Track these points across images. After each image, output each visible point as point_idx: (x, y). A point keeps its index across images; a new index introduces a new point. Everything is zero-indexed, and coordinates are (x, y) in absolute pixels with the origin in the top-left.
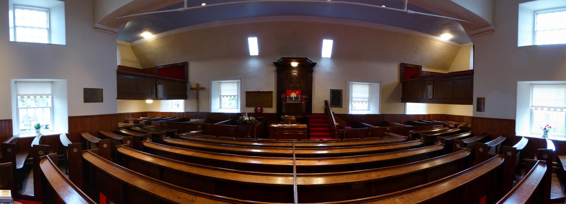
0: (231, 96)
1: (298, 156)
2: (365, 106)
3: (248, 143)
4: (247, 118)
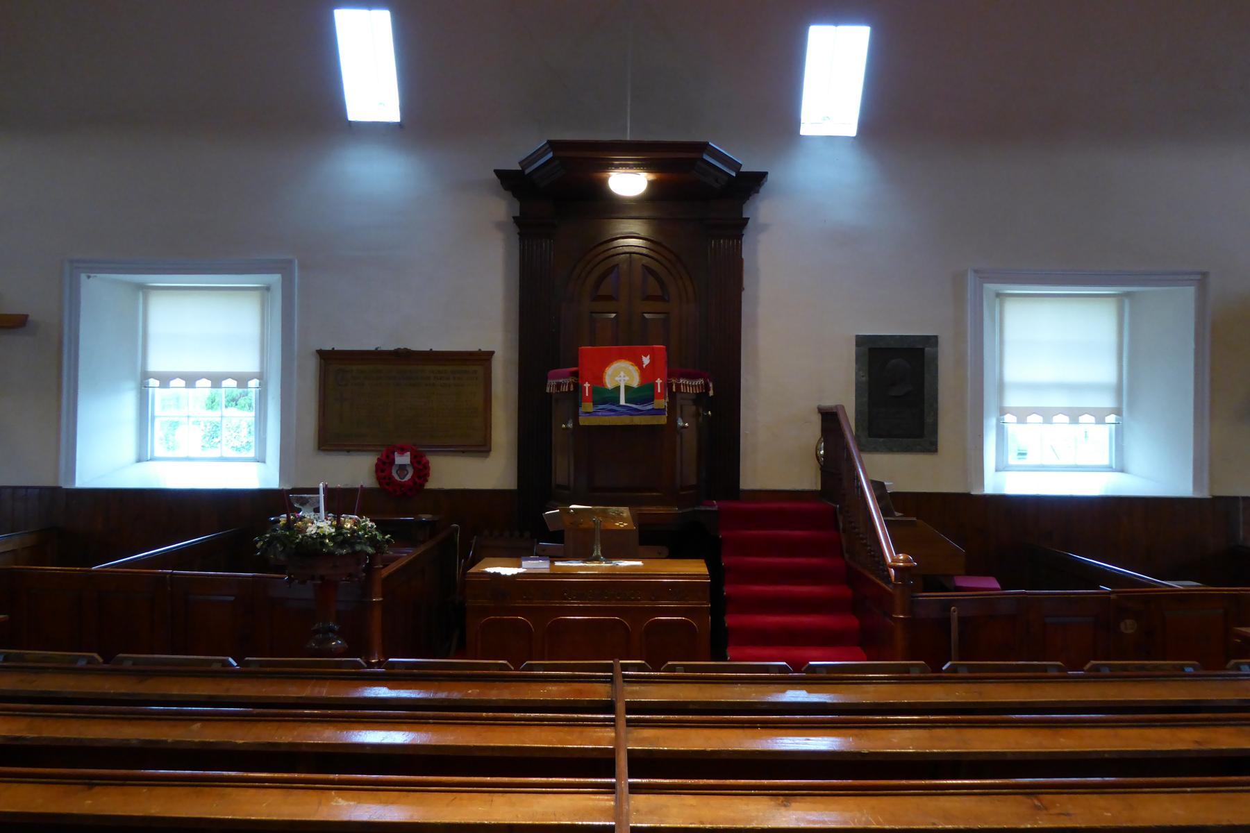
0: (216, 380)
1: (644, 764)
2: (1094, 441)
3: (324, 691)
4: (319, 524)
